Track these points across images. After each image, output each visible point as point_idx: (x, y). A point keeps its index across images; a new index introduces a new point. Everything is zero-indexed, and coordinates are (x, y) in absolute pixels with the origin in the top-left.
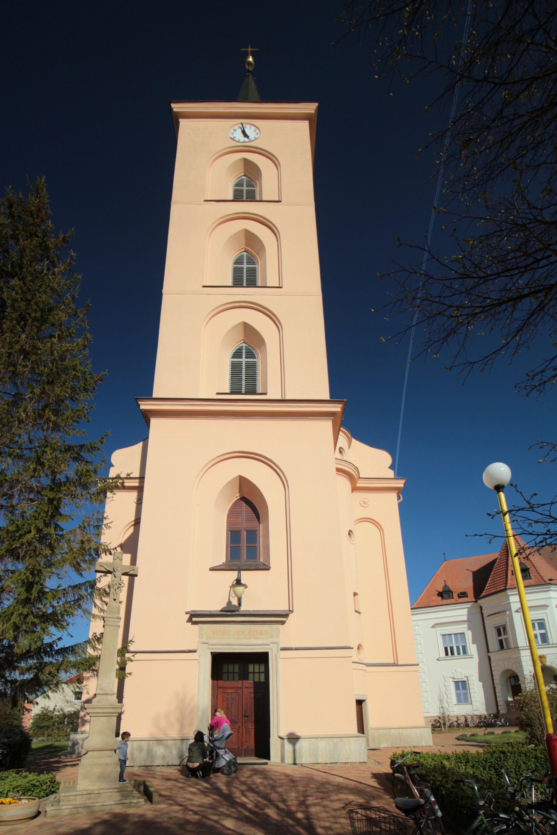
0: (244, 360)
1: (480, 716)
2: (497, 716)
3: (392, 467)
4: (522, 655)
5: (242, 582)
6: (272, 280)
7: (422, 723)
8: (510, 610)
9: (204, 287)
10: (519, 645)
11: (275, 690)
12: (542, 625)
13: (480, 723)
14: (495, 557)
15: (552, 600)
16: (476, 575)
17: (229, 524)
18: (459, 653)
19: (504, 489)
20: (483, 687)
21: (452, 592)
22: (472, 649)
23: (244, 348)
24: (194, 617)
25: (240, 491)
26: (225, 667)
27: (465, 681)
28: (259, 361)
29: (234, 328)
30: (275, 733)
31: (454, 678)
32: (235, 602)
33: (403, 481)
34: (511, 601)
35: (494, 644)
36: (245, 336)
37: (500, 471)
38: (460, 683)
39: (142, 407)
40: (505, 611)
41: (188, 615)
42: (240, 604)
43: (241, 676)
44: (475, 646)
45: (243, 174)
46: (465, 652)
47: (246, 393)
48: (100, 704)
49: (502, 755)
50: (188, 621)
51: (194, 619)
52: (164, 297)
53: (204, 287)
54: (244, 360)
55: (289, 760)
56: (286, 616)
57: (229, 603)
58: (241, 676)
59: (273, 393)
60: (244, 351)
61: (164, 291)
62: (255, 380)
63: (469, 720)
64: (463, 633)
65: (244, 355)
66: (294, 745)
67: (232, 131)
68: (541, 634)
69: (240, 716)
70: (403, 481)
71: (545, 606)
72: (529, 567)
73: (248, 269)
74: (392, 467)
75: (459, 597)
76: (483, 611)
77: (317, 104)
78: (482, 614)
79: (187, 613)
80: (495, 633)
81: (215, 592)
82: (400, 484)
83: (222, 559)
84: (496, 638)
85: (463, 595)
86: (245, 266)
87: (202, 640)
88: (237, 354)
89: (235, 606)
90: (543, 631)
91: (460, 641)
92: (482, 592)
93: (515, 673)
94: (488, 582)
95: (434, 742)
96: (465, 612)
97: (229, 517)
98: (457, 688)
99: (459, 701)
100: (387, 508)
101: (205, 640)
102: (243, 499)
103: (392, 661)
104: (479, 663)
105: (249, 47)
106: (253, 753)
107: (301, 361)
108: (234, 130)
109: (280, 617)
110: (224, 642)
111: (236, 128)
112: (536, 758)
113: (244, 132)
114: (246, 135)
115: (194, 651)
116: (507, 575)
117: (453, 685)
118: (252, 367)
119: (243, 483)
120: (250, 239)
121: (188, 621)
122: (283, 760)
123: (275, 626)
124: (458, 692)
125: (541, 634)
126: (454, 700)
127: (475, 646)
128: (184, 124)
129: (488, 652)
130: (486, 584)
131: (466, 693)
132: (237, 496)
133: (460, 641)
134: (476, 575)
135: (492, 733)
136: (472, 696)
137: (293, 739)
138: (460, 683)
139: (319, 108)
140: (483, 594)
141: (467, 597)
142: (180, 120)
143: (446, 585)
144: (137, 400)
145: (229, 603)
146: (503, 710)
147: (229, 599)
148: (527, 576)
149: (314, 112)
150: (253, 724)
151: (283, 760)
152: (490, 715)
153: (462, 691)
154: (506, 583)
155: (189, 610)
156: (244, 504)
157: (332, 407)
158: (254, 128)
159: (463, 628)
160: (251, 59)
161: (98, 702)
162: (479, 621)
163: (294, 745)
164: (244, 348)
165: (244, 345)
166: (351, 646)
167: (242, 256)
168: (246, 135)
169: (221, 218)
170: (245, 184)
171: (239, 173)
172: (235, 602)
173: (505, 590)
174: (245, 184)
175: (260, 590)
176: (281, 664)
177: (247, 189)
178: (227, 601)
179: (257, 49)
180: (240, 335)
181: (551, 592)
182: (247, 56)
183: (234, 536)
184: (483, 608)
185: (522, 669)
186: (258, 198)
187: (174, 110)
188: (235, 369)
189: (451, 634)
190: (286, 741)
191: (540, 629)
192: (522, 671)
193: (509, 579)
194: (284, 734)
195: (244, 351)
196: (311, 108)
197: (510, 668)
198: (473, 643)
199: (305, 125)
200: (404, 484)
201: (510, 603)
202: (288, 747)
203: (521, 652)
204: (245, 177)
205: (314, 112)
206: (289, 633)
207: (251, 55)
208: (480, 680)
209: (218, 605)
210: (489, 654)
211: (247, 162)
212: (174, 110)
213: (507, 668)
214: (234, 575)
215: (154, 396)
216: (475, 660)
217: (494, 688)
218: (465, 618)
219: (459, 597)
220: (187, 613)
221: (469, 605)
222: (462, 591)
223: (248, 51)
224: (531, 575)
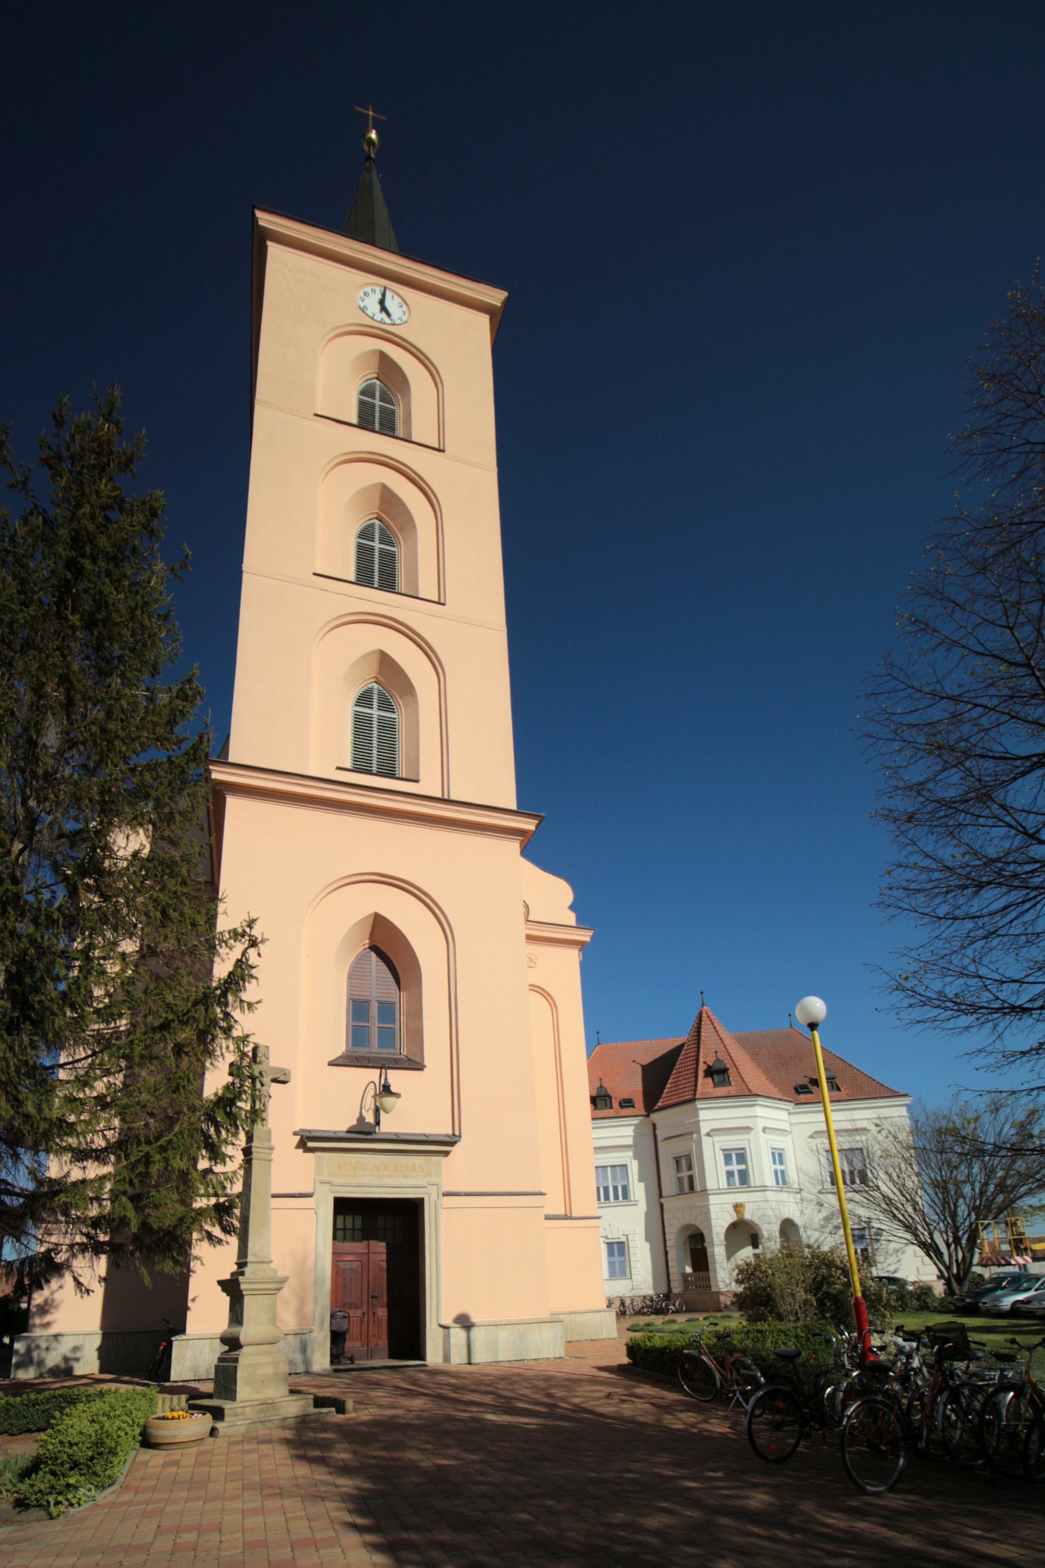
0: (375, 712)
1: (644, 1297)
2: (668, 1296)
3: (572, 908)
4: (711, 1202)
5: (393, 1089)
6: (427, 588)
7: (604, 1304)
8: (698, 1132)
9: (315, 574)
10: (709, 1187)
11: (434, 1257)
12: (742, 1158)
13: (643, 1308)
14: (677, 1044)
15: (758, 1120)
16: (646, 1069)
17: (351, 987)
18: (616, 1198)
19: (819, 1028)
20: (651, 1250)
21: (610, 1097)
22: (638, 1190)
23: (375, 692)
24: (307, 1141)
27: (623, 1243)
28: (401, 716)
29: (364, 656)
30: (434, 1320)
31: (607, 1238)
32: (370, 1118)
33: (590, 933)
34: (701, 1117)
35: (669, 1185)
37: (816, 1006)
38: (616, 1246)
40: (691, 1133)
41: (298, 1138)
42: (378, 1123)
43: (387, 1235)
44: (642, 1185)
45: (375, 375)
46: (625, 1196)
47: (379, 774)
48: (259, 1277)
49: (759, 1335)
50: (297, 1147)
51: (310, 1144)
52: (246, 577)
53: (315, 574)
55: (458, 1358)
56: (452, 1144)
57: (361, 1118)
59: (429, 785)
60: (375, 697)
61: (247, 565)
63: (628, 1302)
64: (625, 1166)
65: (375, 704)
67: (362, 294)
68: (740, 1171)
69: (365, 1297)
70: (590, 933)
71: (748, 1129)
72: (728, 1066)
74: (572, 908)
75: (622, 1107)
76: (657, 1132)
77: (506, 294)
78: (655, 1136)
79: (295, 1134)
80: (672, 1165)
82: (585, 936)
83: (339, 1047)
84: (674, 1176)
85: (627, 1103)
86: (377, 545)
87: (321, 1178)
88: (364, 699)
89: (369, 1124)
90: (743, 1167)
91: (619, 1178)
92: (657, 1101)
93: (698, 1229)
94: (668, 1086)
96: (629, 1131)
97: (350, 977)
98: (611, 1253)
99: (613, 1274)
100: (563, 970)
101: (326, 1178)
103: (562, 1212)
104: (647, 1214)
105: (370, 107)
106: (387, 1354)
107: (471, 731)
108: (365, 294)
112: (797, 1337)
113: (382, 302)
114: (384, 309)
115: (309, 1195)
116: (696, 1077)
117: (604, 1248)
118: (388, 728)
120: (388, 499)
121: (297, 1147)
122: (447, 1358)
124: (612, 1259)
125: (740, 1171)
126: (606, 1275)
127: (642, 1185)
129: (661, 1196)
130: (664, 1088)
131: (624, 1262)
133: (619, 1178)
134: (646, 1069)
135: (674, 1321)
136: (633, 1265)
138: (616, 1246)
139: (507, 300)
140: (659, 1104)
141: (633, 1107)
142: (269, 243)
143: (601, 1086)
145: (361, 1118)
146: (677, 1288)
147: (361, 1113)
148: (724, 1080)
149: (499, 305)
150: (386, 1310)
151: (447, 1358)
152: (659, 1296)
153: (617, 1259)
154: (695, 1090)
155: (297, 1129)
156: (373, 955)
157: (516, 821)
158: (399, 300)
159: (627, 1158)
160: (373, 135)
161: (253, 1273)
162: (650, 1147)
164: (375, 692)
165: (376, 686)
166: (544, 1192)
167: (372, 526)
168: (384, 309)
169: (343, 455)
170: (378, 395)
171: (367, 374)
172: (370, 1118)
173: (693, 1100)
174: (378, 395)
175: (417, 1104)
178: (357, 1115)
179: (384, 118)
180: (372, 670)
181: (757, 1108)
182: (367, 131)
184: (658, 1126)
185: (710, 1223)
186: (400, 432)
187: (261, 223)
188: (361, 724)
189: (606, 1167)
191: (738, 1163)
192: (710, 1227)
193: (699, 1083)
195: (375, 697)
196: (496, 297)
197: (692, 1222)
198: (640, 1180)
200: (592, 938)
201: (698, 1122)
202: (458, 1335)
203: (711, 1197)
204: (378, 382)
205: (499, 305)
206: (456, 1169)
207: (374, 128)
208: (647, 1239)
209: (342, 1122)
210: (662, 1200)
211: (384, 359)
213: (688, 1222)
216: (642, 1207)
217: (666, 1253)
218: (630, 1141)
219: (622, 1107)
220: (295, 1134)
221: (636, 1121)
222: (626, 1097)
224: (731, 1079)
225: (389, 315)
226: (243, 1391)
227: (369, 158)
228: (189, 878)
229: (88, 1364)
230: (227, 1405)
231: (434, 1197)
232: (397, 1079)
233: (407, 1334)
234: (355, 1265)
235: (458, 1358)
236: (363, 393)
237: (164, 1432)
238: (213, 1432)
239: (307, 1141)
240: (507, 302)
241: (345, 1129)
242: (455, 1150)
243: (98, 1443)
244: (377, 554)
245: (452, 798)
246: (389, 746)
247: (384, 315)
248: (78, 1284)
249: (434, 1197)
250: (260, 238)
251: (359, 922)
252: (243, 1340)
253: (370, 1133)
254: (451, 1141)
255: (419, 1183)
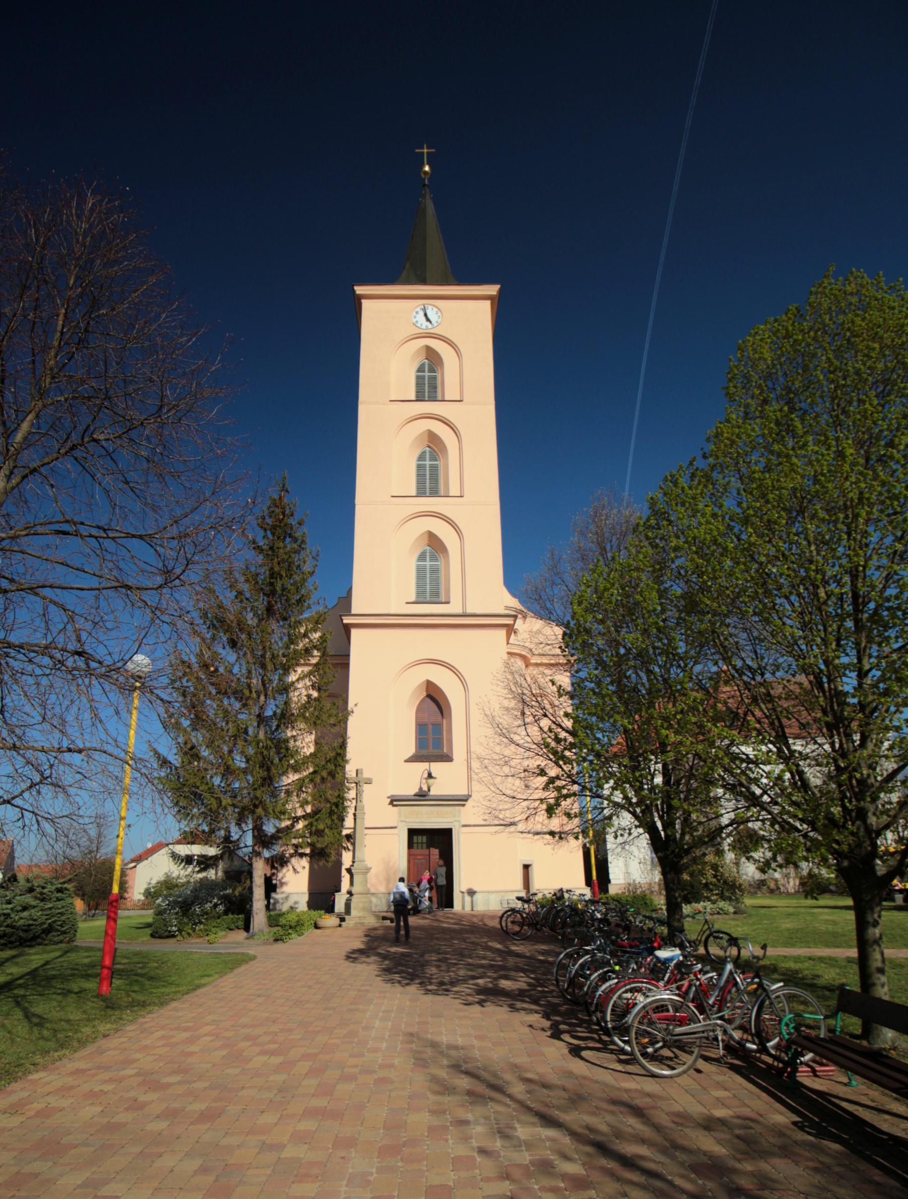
5: (433, 775)
6: (454, 490)
24: (394, 801)
25: (427, 690)
26: (415, 838)
36: (429, 541)
39: (345, 621)
43: (434, 846)
51: (395, 803)
54: (428, 563)
55: (468, 908)
56: (466, 800)
57: (421, 788)
58: (432, 845)
60: (428, 555)
62: (438, 584)
65: (428, 559)
66: (472, 897)
67: (414, 314)
73: (431, 466)
77: (499, 286)
81: (410, 779)
83: (411, 750)
95: (341, 855)
102: (429, 696)
108: (417, 313)
109: (461, 800)
110: (418, 820)
111: (418, 309)
113: (426, 315)
114: (428, 320)
115: (395, 828)
119: (429, 685)
120: (433, 439)
122: (463, 908)
123: (457, 808)
128: (365, 303)
132: (425, 694)
137: (471, 893)
144: (341, 616)
145: (421, 788)
151: (463, 908)
156: (429, 700)
160: (427, 168)
163: (472, 897)
168: (428, 320)
171: (422, 359)
172: (425, 788)
176: (462, 837)
177: (428, 386)
183: (421, 728)
188: (420, 572)
190: (466, 895)
194: (464, 889)
195: (428, 555)
196: (493, 290)
199: (487, 304)
202: (468, 898)
209: (412, 791)
212: (358, 292)
214: (424, 766)
215: (353, 612)
223: (423, 153)
225: (431, 322)
226: (354, 912)
227: (424, 185)
228: (335, 664)
229: (303, 906)
230: (347, 917)
231: (457, 827)
232: (436, 768)
233: (445, 895)
234: (423, 861)
235: (468, 908)
236: (418, 371)
237: (322, 923)
238: (340, 926)
239: (394, 801)
240: (500, 291)
241: (413, 793)
242: (469, 803)
243: (298, 921)
244: (428, 468)
245: (469, 610)
246: (436, 582)
247: (428, 323)
248: (294, 869)
249: (457, 827)
250: (355, 305)
251: (419, 685)
252: (353, 892)
253: (424, 796)
254: (469, 796)
255: (450, 820)
